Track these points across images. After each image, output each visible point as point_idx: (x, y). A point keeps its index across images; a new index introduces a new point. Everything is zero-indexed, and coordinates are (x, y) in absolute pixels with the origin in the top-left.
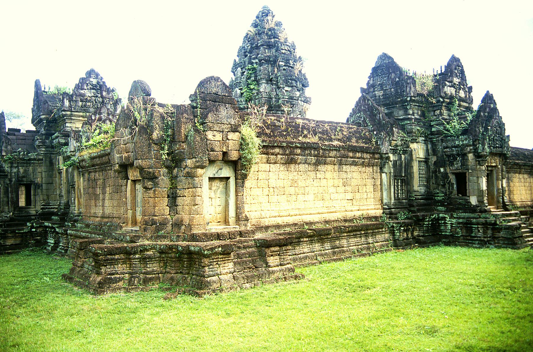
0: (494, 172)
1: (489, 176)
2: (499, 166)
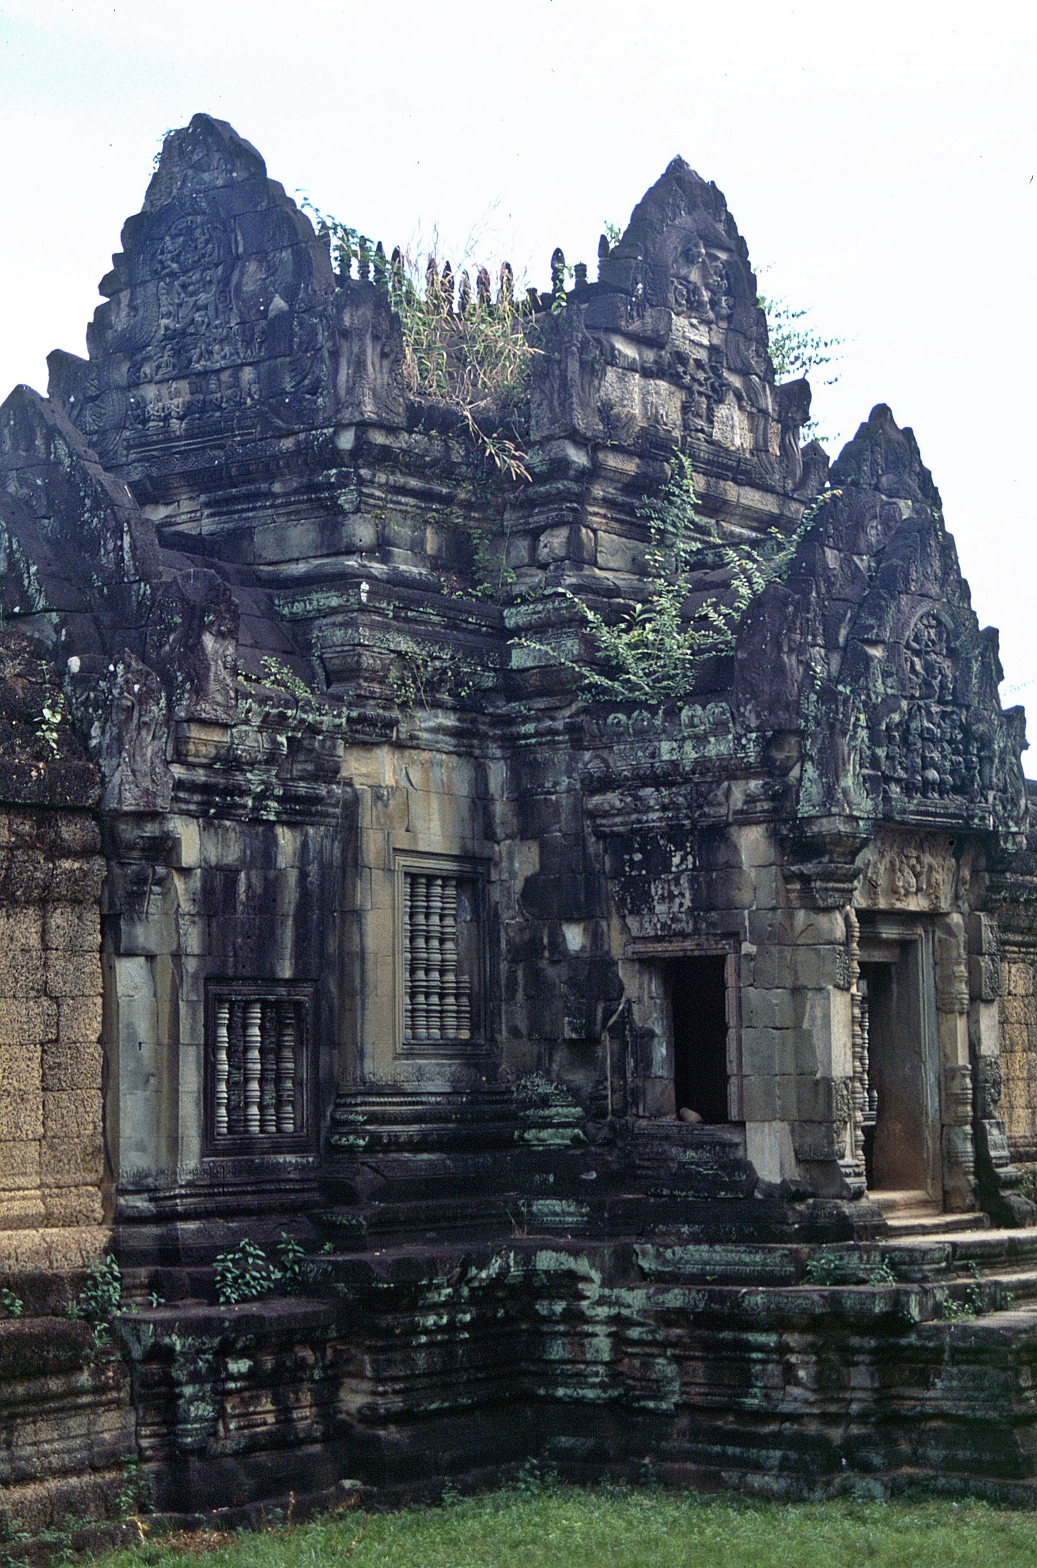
0: (925, 956)
1: (884, 990)
2: (956, 918)
